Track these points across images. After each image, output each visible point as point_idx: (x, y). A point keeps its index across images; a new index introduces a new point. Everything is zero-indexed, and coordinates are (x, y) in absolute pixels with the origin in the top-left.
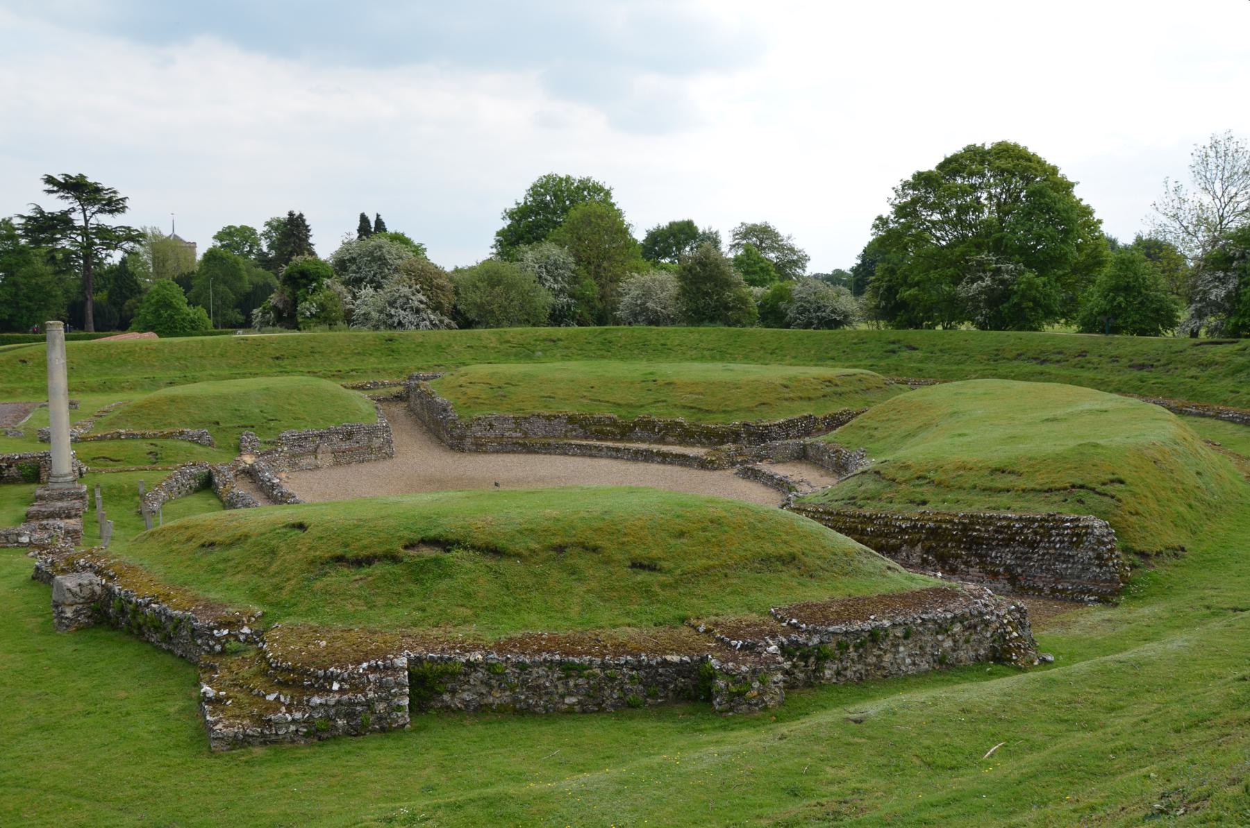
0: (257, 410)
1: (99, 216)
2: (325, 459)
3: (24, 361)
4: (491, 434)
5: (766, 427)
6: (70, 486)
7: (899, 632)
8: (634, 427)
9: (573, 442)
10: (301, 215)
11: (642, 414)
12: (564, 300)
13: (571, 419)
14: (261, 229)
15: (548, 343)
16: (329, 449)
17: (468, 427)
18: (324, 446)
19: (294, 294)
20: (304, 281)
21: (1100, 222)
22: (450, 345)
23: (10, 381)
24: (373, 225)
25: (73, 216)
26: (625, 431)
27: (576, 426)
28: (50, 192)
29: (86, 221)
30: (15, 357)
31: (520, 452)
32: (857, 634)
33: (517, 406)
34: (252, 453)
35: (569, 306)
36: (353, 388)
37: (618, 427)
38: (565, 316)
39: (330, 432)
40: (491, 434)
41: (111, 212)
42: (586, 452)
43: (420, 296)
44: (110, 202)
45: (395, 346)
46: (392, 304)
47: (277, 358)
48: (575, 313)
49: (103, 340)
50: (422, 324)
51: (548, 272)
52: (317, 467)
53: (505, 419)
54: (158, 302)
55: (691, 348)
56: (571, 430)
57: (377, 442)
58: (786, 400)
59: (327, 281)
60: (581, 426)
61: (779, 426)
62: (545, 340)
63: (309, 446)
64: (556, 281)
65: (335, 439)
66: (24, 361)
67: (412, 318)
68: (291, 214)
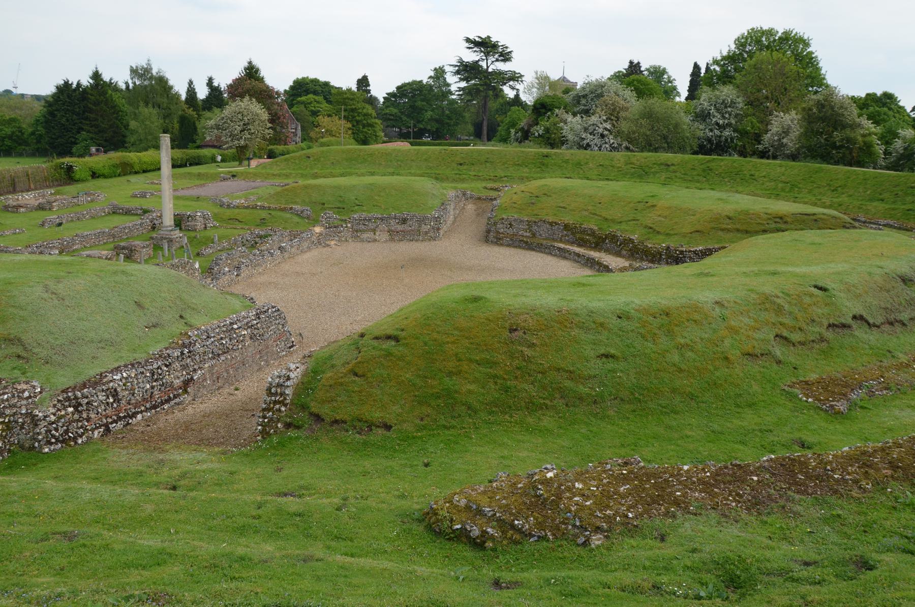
1: (497, 63)
2: (383, 236)
4: (510, 231)
8: (606, 238)
9: (556, 244)
10: (639, 63)
11: (613, 229)
12: (727, 133)
13: (566, 227)
14: (529, 77)
16: (386, 228)
17: (495, 224)
19: (536, 119)
20: (543, 111)
24: (703, 71)
25: (480, 63)
26: (599, 242)
27: (569, 233)
28: (469, 48)
31: (524, 248)
33: (535, 212)
34: (323, 225)
35: (732, 139)
36: (491, 189)
39: (390, 218)
40: (510, 231)
42: (563, 254)
43: (605, 125)
44: (501, 55)
45: (546, 161)
46: (586, 130)
47: (461, 164)
48: (736, 145)
51: (718, 110)
52: (375, 240)
53: (521, 221)
55: (771, 180)
56: (566, 235)
57: (425, 228)
58: (722, 230)
59: (557, 111)
60: (573, 234)
61: (695, 252)
62: (662, 164)
63: (371, 225)
64: (724, 118)
65: (392, 222)
67: (597, 141)
68: (631, 62)
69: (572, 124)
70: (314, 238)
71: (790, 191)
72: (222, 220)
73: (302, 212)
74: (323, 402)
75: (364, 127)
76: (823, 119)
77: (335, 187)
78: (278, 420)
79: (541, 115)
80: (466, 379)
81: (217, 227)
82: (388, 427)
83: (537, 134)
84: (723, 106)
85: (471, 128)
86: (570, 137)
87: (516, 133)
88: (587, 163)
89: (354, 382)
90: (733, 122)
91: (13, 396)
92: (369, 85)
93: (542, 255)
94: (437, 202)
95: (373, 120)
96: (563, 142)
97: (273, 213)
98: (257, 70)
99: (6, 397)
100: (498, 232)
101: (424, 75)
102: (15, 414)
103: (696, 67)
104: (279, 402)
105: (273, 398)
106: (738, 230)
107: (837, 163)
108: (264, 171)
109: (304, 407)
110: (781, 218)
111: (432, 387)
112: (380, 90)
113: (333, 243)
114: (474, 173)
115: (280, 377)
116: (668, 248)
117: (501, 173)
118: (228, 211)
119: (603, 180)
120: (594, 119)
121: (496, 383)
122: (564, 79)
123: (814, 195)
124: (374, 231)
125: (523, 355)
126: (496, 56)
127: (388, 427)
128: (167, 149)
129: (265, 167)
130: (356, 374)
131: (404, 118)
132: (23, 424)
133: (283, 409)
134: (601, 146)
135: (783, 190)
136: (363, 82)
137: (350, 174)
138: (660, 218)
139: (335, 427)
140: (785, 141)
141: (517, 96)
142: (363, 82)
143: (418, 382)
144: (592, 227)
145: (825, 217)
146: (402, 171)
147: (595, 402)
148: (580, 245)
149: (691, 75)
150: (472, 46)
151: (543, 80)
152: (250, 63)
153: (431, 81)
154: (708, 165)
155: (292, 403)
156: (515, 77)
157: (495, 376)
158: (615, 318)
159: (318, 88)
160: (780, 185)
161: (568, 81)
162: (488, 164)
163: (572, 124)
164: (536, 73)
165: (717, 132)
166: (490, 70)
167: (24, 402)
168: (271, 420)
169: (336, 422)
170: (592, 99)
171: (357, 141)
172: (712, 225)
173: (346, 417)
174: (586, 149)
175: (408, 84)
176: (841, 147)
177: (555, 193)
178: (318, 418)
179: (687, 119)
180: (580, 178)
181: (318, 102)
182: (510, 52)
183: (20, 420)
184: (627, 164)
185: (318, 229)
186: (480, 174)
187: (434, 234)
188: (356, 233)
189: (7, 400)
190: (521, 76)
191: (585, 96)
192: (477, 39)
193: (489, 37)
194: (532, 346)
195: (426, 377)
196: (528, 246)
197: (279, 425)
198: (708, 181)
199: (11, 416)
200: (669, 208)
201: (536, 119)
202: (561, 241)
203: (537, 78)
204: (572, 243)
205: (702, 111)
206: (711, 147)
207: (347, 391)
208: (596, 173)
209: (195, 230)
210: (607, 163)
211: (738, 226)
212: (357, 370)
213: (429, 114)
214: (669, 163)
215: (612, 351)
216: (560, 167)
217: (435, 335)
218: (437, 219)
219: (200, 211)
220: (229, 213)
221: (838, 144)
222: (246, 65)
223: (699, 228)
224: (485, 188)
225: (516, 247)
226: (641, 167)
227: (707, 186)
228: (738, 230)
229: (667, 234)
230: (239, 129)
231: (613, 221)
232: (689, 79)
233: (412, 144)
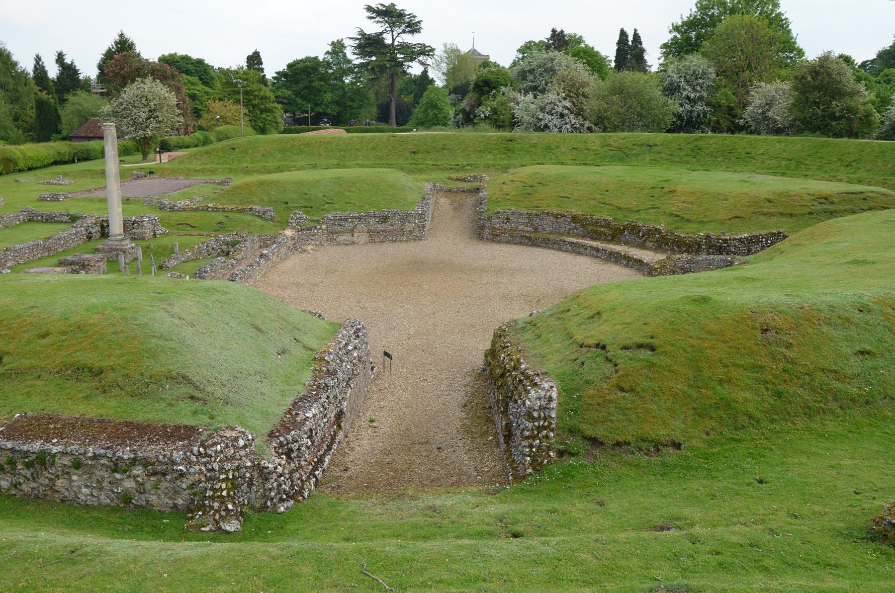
0: (321, 195)
2: (361, 237)
3: (234, 149)
4: (507, 226)
5: (725, 241)
6: (116, 243)
7: (66, 461)
8: (624, 230)
11: (632, 218)
12: (699, 107)
13: (574, 219)
15: (644, 148)
17: (490, 218)
18: (361, 226)
19: (479, 99)
20: (487, 89)
21: (562, 31)
22: (557, 147)
23: (218, 163)
24: (631, 38)
25: (385, 36)
26: (616, 234)
27: (578, 225)
29: (394, 40)
30: (228, 145)
31: (527, 245)
32: (26, 454)
33: (535, 204)
34: (294, 228)
35: (705, 113)
36: (457, 180)
37: (611, 228)
38: (702, 124)
39: (368, 216)
40: (507, 226)
41: (412, 32)
42: (577, 250)
44: (409, 25)
45: (511, 145)
46: (542, 109)
47: (414, 153)
48: (710, 120)
49: (310, 134)
50: (564, 127)
51: (687, 82)
52: (353, 243)
53: (520, 214)
54: (427, 103)
55: (771, 158)
56: (574, 228)
57: (409, 227)
58: (764, 214)
59: (503, 89)
60: (583, 226)
61: (740, 240)
62: (642, 145)
63: (348, 226)
64: (695, 90)
65: (372, 221)
66: (234, 149)
67: (556, 121)
68: (554, 31)
69: (524, 104)
70: (290, 243)
71: (796, 169)
72: (169, 226)
73: (264, 213)
74: (596, 423)
75: (262, 112)
76: (819, 88)
77: (296, 183)
78: (549, 448)
79: (483, 94)
80: (738, 386)
81: (168, 235)
82: (677, 446)
83: (483, 116)
84: (693, 78)
85: (374, 110)
86: (526, 118)
87: (456, 115)
88: (557, 147)
89: (624, 398)
90: (705, 95)
91: (227, 446)
92: (262, 64)
93: (552, 251)
94: (416, 197)
95: (273, 105)
96: (513, 123)
97: (230, 215)
98: (131, 46)
99: (219, 447)
100: (493, 228)
101: (320, 51)
102: (238, 469)
103: (623, 34)
104: (545, 428)
105: (536, 424)
106: (782, 214)
107: (837, 135)
108: (182, 166)
109: (572, 431)
110: (826, 198)
111: (707, 397)
112: (271, 68)
113: (310, 247)
114: (432, 163)
115: (540, 399)
116: (708, 237)
117: (462, 161)
118: (171, 214)
119: (580, 165)
120: (551, 97)
121: (767, 389)
122: (474, 52)
123: (826, 172)
124: (352, 232)
125: (785, 357)
126: (403, 27)
127: (677, 446)
128: (113, 142)
129: (182, 162)
130: (622, 390)
131: (300, 101)
132: (251, 479)
133: (552, 434)
134: (561, 127)
135: (788, 168)
136: (255, 60)
137: (344, 166)
138: (685, 205)
139: (617, 450)
140: (770, 114)
141: (425, 73)
142: (255, 60)
143: (694, 394)
144: (606, 217)
145: (874, 195)
146: (330, 161)
147: (867, 403)
148: (593, 239)
149: (618, 44)
150: (374, 15)
151: (453, 55)
152: (121, 36)
153: (329, 58)
154: (696, 143)
155: (558, 428)
156: (426, 51)
157: (766, 382)
158: (857, 312)
159: (190, 67)
160: (784, 163)
161: (479, 54)
162: (445, 152)
163: (524, 104)
164: (445, 46)
165: (688, 107)
166: (396, 43)
167: (242, 453)
168: (539, 448)
169: (618, 444)
170: (541, 74)
171: (255, 129)
172: (753, 209)
173: (629, 438)
174: (543, 130)
175: (301, 61)
176: (841, 118)
177: (550, 182)
178: (595, 442)
179: (657, 93)
180: (553, 164)
181: (193, 84)
182: (419, 22)
183: (248, 475)
184: (603, 146)
185: (289, 233)
186: (439, 163)
187: (418, 233)
188: (331, 236)
189: (221, 452)
190: (433, 50)
191: (531, 71)
192: (380, 8)
193: (393, 5)
194: (789, 346)
195: (699, 387)
196: (533, 242)
197: (551, 454)
198: (698, 161)
199: (233, 471)
200: (693, 193)
201: (479, 99)
202: (569, 235)
203: (446, 52)
204: (583, 237)
205: (671, 84)
206: (686, 124)
207: (621, 409)
208: (570, 157)
209: (144, 239)
210: (580, 146)
211: (781, 210)
212: (623, 384)
213: (328, 96)
214: (651, 143)
215: (868, 348)
216: (528, 152)
217: (691, 341)
218: (422, 216)
219: (149, 216)
220: (175, 217)
221: (837, 114)
222: (118, 38)
223: (739, 214)
224: (450, 178)
225: (516, 244)
226: (620, 149)
227: (699, 167)
228: (782, 214)
229: (700, 222)
230: (144, 116)
231: (628, 210)
232: (616, 47)
233: (348, 131)
